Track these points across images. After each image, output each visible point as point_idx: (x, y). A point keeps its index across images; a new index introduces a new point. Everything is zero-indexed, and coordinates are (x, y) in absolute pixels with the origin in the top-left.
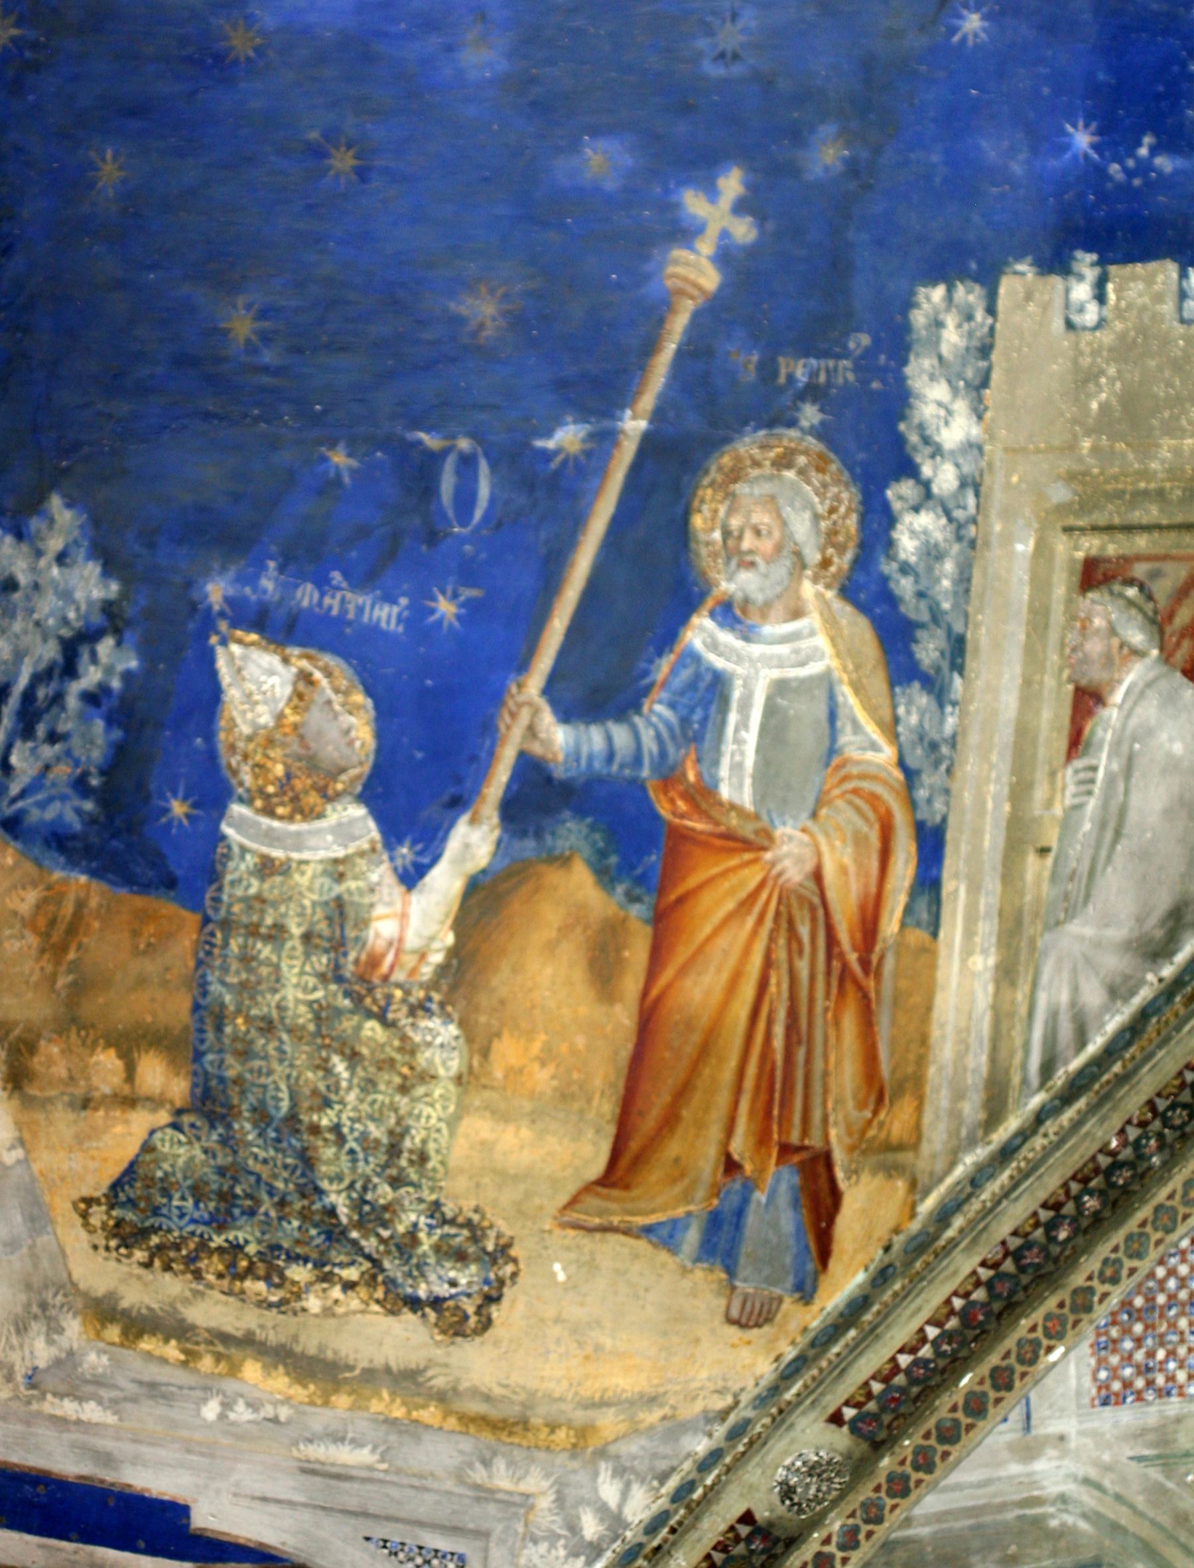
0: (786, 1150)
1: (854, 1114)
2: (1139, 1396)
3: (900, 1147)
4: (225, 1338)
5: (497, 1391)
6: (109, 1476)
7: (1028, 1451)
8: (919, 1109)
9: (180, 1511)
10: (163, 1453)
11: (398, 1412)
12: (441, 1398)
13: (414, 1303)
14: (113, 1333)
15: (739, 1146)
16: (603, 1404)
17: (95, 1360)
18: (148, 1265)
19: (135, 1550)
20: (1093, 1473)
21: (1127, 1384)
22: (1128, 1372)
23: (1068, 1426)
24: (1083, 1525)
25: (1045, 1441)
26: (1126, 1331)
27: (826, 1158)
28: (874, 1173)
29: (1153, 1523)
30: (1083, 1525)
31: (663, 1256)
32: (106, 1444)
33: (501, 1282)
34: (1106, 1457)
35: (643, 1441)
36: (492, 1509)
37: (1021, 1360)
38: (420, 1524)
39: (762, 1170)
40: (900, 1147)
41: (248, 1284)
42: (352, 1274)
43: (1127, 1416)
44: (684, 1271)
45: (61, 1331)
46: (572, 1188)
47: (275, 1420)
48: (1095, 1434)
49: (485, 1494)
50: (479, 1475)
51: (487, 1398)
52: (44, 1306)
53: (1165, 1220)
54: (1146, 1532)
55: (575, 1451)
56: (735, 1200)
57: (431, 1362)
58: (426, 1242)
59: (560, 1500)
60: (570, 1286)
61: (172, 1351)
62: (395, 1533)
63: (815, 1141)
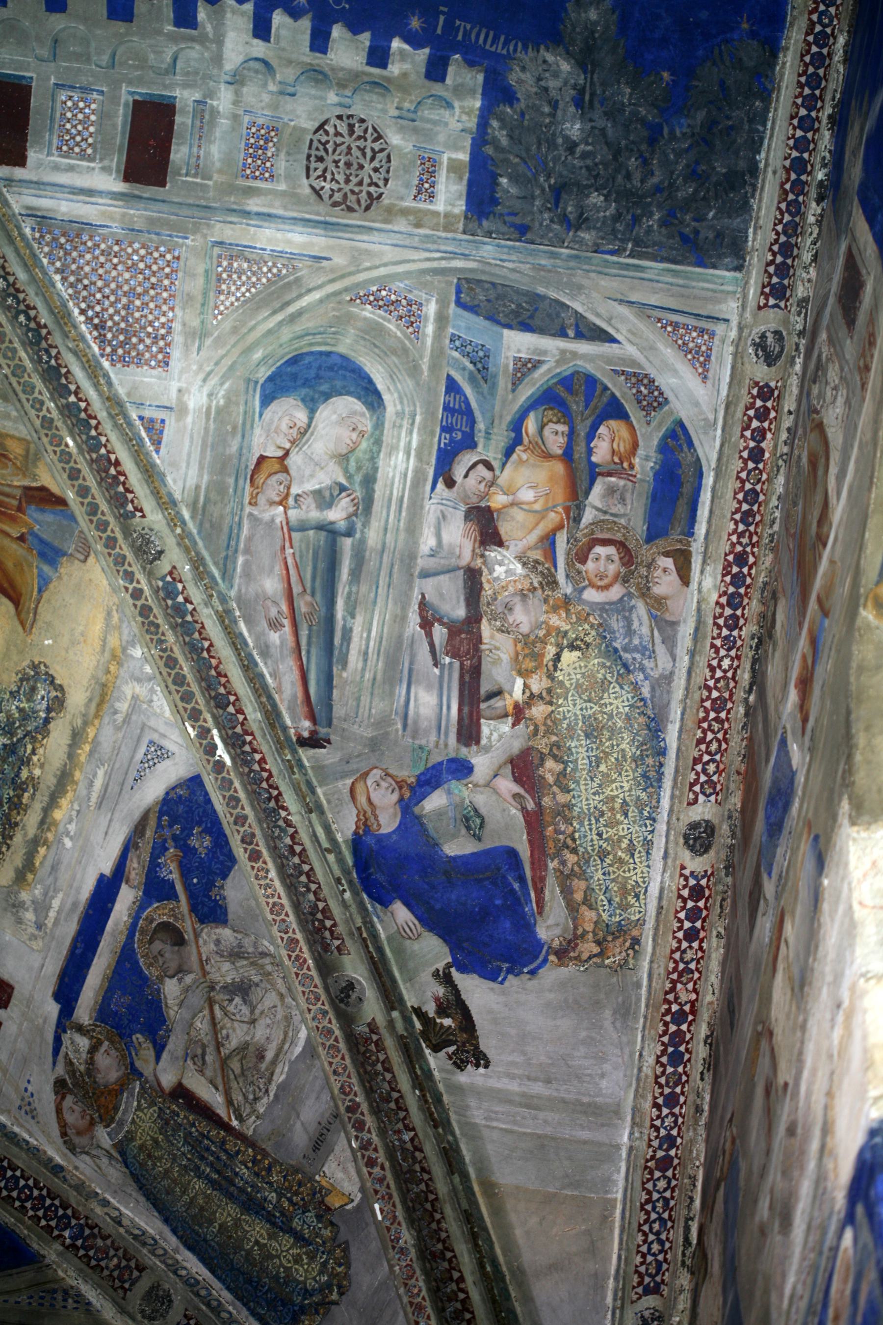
0: (20, 509)
1: (9, 471)
2: (168, 345)
3: (27, 451)
4: (42, 822)
5: (88, 694)
6: (81, 908)
7: (181, 410)
8: (12, 437)
9: (102, 878)
10: (79, 876)
11: (87, 748)
12: (86, 724)
13: (47, 721)
14: (30, 877)
15: (15, 534)
16: (104, 641)
17: (38, 892)
18: (9, 847)
19: (111, 910)
20: (201, 376)
21: (161, 350)
22: (154, 349)
23: (174, 386)
24: (226, 386)
25: (179, 400)
26: (135, 346)
27: (27, 489)
28: (36, 467)
29: (233, 346)
30: (226, 386)
31: (51, 586)
32: (68, 905)
33: (47, 674)
34: (194, 367)
35: (124, 625)
36: (134, 717)
37: (68, 462)
38: (132, 757)
39: (26, 524)
40: (27, 451)
41: (24, 801)
42: (29, 747)
43: (176, 353)
44: (60, 578)
45: (24, 902)
46: (17, 623)
47: (78, 812)
48: (181, 373)
49: (127, 719)
50: (119, 718)
51: (90, 700)
52: (14, 906)
53: (19, 372)
54: (237, 351)
55: (120, 664)
56: (36, 541)
57: (71, 723)
58: (24, 705)
59: (139, 680)
60: (55, 638)
61: (42, 850)
62: (133, 774)
63: (18, 493)
